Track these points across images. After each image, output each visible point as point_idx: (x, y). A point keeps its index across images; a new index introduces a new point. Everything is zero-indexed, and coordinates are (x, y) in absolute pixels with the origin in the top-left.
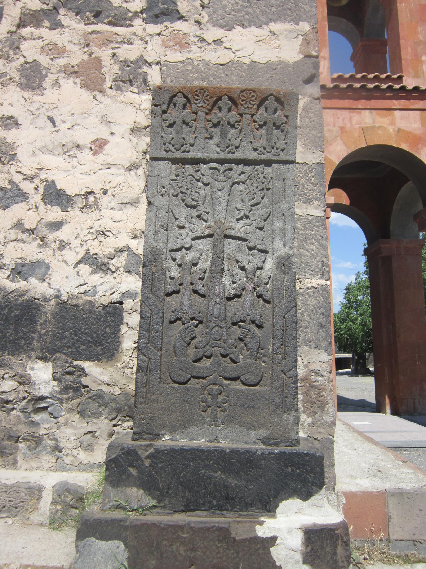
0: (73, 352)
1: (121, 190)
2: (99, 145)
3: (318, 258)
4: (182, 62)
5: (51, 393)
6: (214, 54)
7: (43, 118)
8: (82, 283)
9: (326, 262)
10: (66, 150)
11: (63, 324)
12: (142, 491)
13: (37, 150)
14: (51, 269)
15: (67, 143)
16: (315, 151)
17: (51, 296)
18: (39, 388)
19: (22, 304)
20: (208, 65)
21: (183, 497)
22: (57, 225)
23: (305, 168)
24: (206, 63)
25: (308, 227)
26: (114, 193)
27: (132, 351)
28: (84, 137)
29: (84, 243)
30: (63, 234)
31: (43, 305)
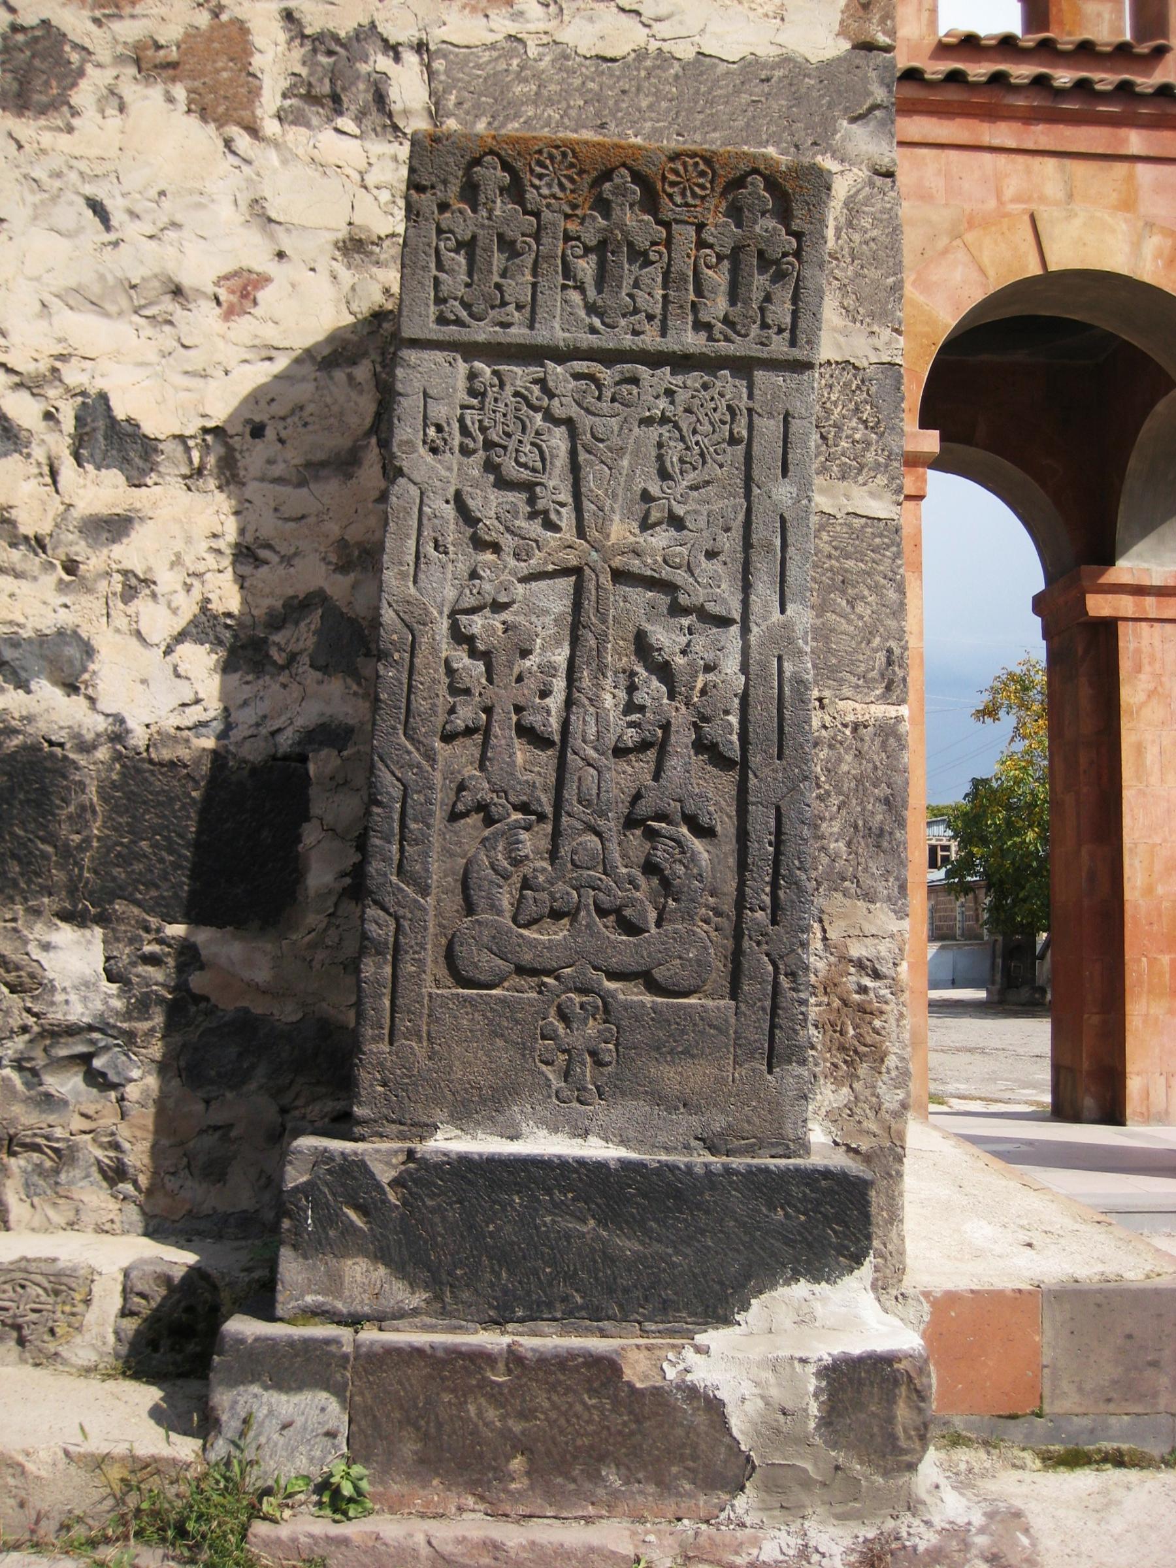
0: (164, 898)
1: (306, 425)
2: (244, 290)
3: (877, 641)
4: (493, 46)
5: (101, 1015)
6: (589, 28)
7: (71, 204)
8: (188, 697)
9: (897, 651)
10: (143, 302)
11: (133, 817)
12: (382, 1271)
13: (56, 300)
14: (98, 658)
15: (143, 279)
16: (875, 328)
17: (98, 735)
18: (67, 1002)
19: (12, 756)
20: (566, 57)
21: (492, 1285)
22: (112, 527)
23: (846, 377)
24: (564, 56)
25: (850, 548)
26: (283, 434)
27: (334, 898)
28: (200, 268)
29: (196, 583)
30: (130, 553)
31: (74, 762)
